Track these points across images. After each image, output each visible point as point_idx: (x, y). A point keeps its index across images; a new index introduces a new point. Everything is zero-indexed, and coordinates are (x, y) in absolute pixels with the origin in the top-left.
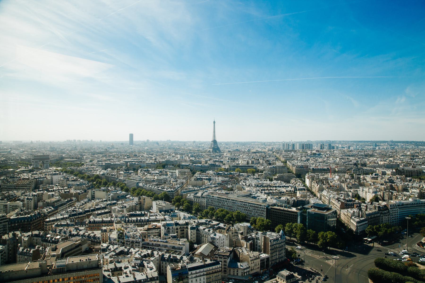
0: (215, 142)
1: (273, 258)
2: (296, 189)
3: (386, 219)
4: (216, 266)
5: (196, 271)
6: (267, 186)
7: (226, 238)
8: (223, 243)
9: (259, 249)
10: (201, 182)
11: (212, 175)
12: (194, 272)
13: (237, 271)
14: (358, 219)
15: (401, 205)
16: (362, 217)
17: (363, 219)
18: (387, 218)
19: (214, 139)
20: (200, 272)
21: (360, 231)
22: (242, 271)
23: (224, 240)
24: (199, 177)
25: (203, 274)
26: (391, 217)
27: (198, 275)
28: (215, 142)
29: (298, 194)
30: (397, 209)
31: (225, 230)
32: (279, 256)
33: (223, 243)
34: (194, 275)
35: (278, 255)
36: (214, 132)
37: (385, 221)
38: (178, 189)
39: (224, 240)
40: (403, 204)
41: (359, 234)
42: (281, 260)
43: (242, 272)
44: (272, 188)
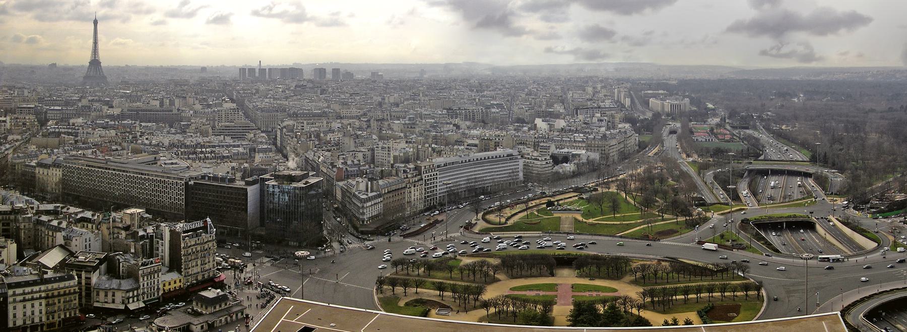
0: (95, 63)
1: (190, 270)
2: (253, 150)
3: (416, 197)
4: (67, 283)
5: (24, 289)
6: (207, 158)
7: (95, 238)
8: (88, 246)
9: (162, 256)
10: (57, 140)
11: (81, 126)
12: (19, 291)
13: (113, 295)
14: (365, 195)
15: (443, 165)
16: (372, 191)
17: (374, 194)
18: (417, 195)
19: (95, 57)
20: (32, 292)
21: (368, 216)
22: (124, 295)
23: (90, 241)
24: (54, 130)
25: (38, 296)
26: (425, 188)
27: (28, 297)
28: (95, 63)
29: (258, 158)
30: (435, 173)
31: (94, 223)
32: (202, 267)
33: (88, 246)
34: (21, 298)
35: (199, 265)
36: (95, 43)
37: (414, 200)
38: (6, 153)
39: (90, 241)
40: (447, 163)
41: (367, 221)
42: (206, 276)
43: (122, 297)
44: (204, 150)
